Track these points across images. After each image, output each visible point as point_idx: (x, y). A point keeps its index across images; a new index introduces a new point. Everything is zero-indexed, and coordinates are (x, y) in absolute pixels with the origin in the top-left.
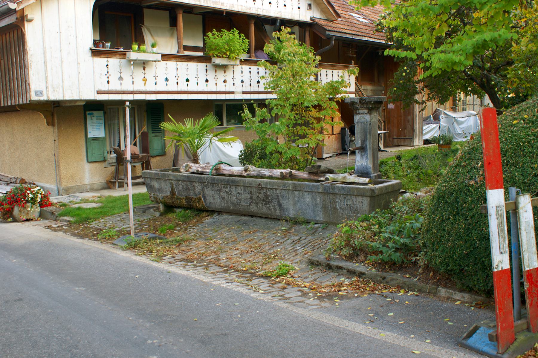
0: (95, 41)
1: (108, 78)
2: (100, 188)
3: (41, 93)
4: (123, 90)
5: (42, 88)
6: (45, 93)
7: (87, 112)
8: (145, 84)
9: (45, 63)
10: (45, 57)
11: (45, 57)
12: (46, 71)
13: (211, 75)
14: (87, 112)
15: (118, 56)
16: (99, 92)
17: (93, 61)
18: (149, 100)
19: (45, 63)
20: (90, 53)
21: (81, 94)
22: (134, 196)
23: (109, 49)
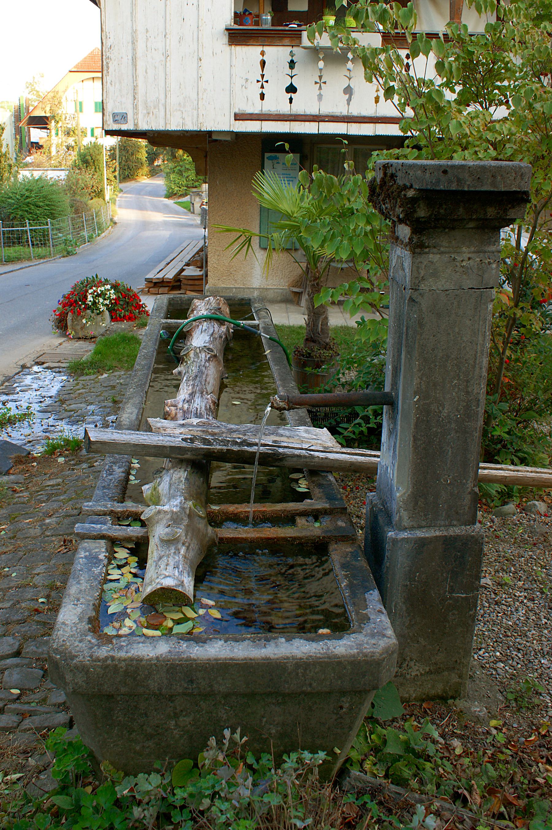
0: (235, 13)
1: (262, 87)
2: (279, 298)
3: (124, 117)
4: (293, 112)
5: (127, 107)
6: (130, 117)
7: (267, 155)
8: (349, 101)
9: (134, 60)
10: (134, 49)
11: (134, 49)
12: (135, 77)
13: (304, 82)
14: (267, 155)
15: (287, 41)
16: (239, 117)
17: (231, 54)
18: (327, 134)
19: (134, 60)
20: (226, 39)
21: (201, 120)
22: (257, 327)
23: (268, 26)
